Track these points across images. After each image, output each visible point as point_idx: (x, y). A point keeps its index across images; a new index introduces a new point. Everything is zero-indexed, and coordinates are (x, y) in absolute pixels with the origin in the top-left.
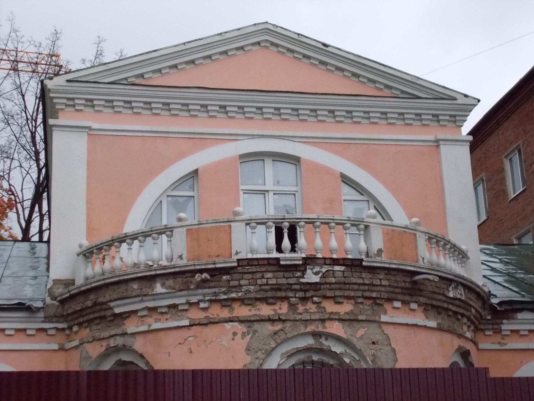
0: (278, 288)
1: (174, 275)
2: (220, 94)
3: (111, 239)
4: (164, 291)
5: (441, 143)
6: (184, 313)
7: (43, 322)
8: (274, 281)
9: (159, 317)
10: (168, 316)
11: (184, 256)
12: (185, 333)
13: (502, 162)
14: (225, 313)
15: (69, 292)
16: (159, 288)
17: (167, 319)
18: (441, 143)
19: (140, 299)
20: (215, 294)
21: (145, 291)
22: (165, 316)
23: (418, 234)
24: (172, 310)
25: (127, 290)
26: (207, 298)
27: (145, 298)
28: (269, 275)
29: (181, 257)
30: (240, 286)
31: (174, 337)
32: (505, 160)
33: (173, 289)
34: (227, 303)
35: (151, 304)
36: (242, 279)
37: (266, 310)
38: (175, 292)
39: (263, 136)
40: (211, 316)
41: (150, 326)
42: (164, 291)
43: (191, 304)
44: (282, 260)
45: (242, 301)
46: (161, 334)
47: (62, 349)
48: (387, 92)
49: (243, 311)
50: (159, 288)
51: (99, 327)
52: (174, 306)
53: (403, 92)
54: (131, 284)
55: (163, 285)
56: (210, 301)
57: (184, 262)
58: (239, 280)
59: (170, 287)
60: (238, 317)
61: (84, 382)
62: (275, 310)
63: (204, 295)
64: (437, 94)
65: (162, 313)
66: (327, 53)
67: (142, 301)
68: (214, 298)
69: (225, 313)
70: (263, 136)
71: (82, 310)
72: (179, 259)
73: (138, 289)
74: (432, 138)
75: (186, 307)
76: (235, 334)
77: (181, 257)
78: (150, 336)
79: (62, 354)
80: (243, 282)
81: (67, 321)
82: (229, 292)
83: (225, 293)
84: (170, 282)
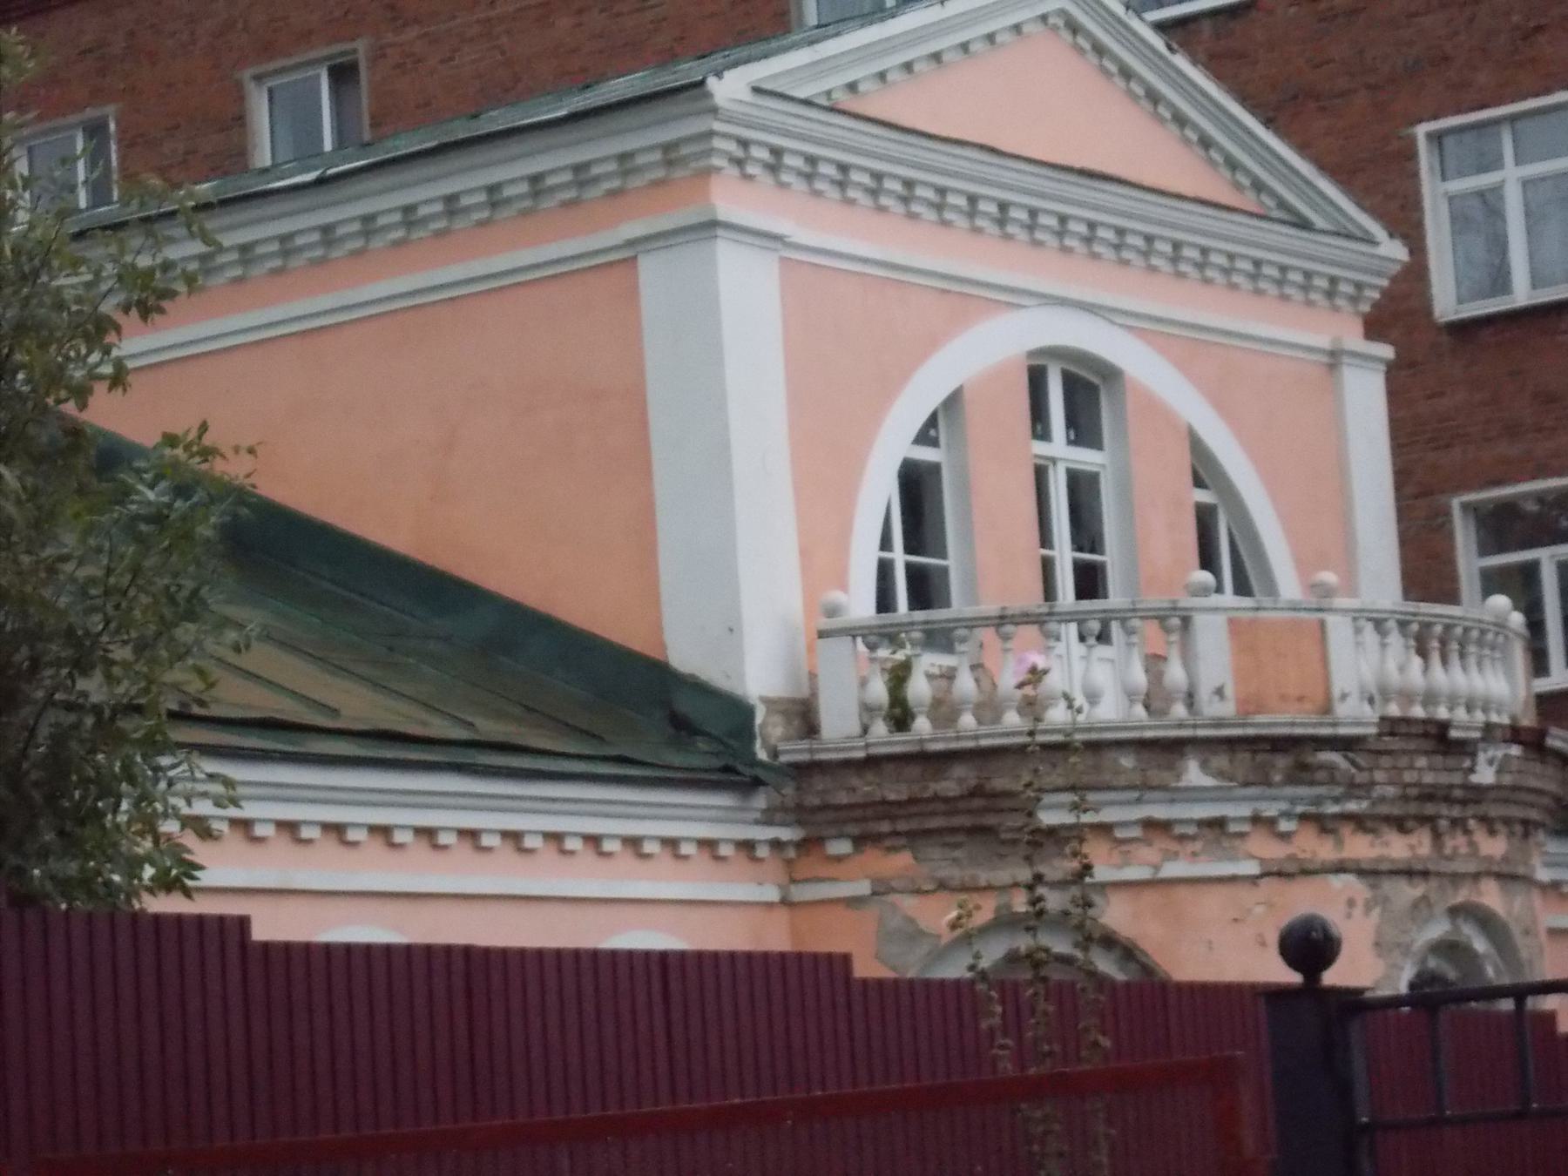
0: (1429, 795)
1: (1231, 743)
2: (935, 151)
3: (994, 613)
4: (1209, 781)
5: (1346, 359)
6: (1237, 843)
7: (757, 822)
8: (1429, 778)
9: (1174, 846)
10: (1198, 846)
11: (1229, 691)
12: (1245, 894)
13: (241, 98)
14: (1325, 850)
15: (867, 746)
16: (1194, 774)
17: (1194, 854)
18: (1346, 359)
19: (1136, 794)
20: (1318, 801)
21: (1156, 776)
22: (1191, 847)
23: (1331, 619)
24: (1206, 831)
25: (1097, 768)
26: (1300, 809)
27: (1149, 795)
28: (1422, 762)
29: (1219, 692)
30: (1373, 784)
31: (1212, 903)
32: (251, 86)
33: (1231, 780)
34: (1324, 824)
35: (1160, 812)
36: (1378, 768)
37: (1397, 847)
38: (1230, 788)
39: (1063, 302)
40: (1301, 856)
41: (1157, 868)
42: (1209, 781)
43: (1256, 820)
44: (1457, 728)
45: (1360, 822)
46: (1183, 892)
47: (785, 902)
48: (1248, 201)
49: (1359, 847)
50: (1194, 774)
51: (957, 853)
52: (1218, 824)
53: (1282, 204)
54: (1111, 755)
55: (1204, 766)
56: (1304, 818)
57: (1227, 709)
58: (1371, 770)
59: (1220, 774)
60: (1357, 861)
61: (459, 964)
62: (1412, 847)
63: (1293, 801)
64: (1342, 220)
65: (1182, 838)
66: (1179, 80)
67: (1139, 801)
68: (1312, 809)
69: (1325, 850)
70: (1063, 302)
71: (912, 801)
72: (1216, 698)
73: (1134, 769)
74: (1323, 341)
75: (1246, 828)
76: (1351, 903)
77: (1219, 692)
78: (1150, 897)
79: (782, 915)
80: (1379, 776)
81: (800, 823)
82: (1348, 796)
83: (1336, 800)
84: (1221, 761)
